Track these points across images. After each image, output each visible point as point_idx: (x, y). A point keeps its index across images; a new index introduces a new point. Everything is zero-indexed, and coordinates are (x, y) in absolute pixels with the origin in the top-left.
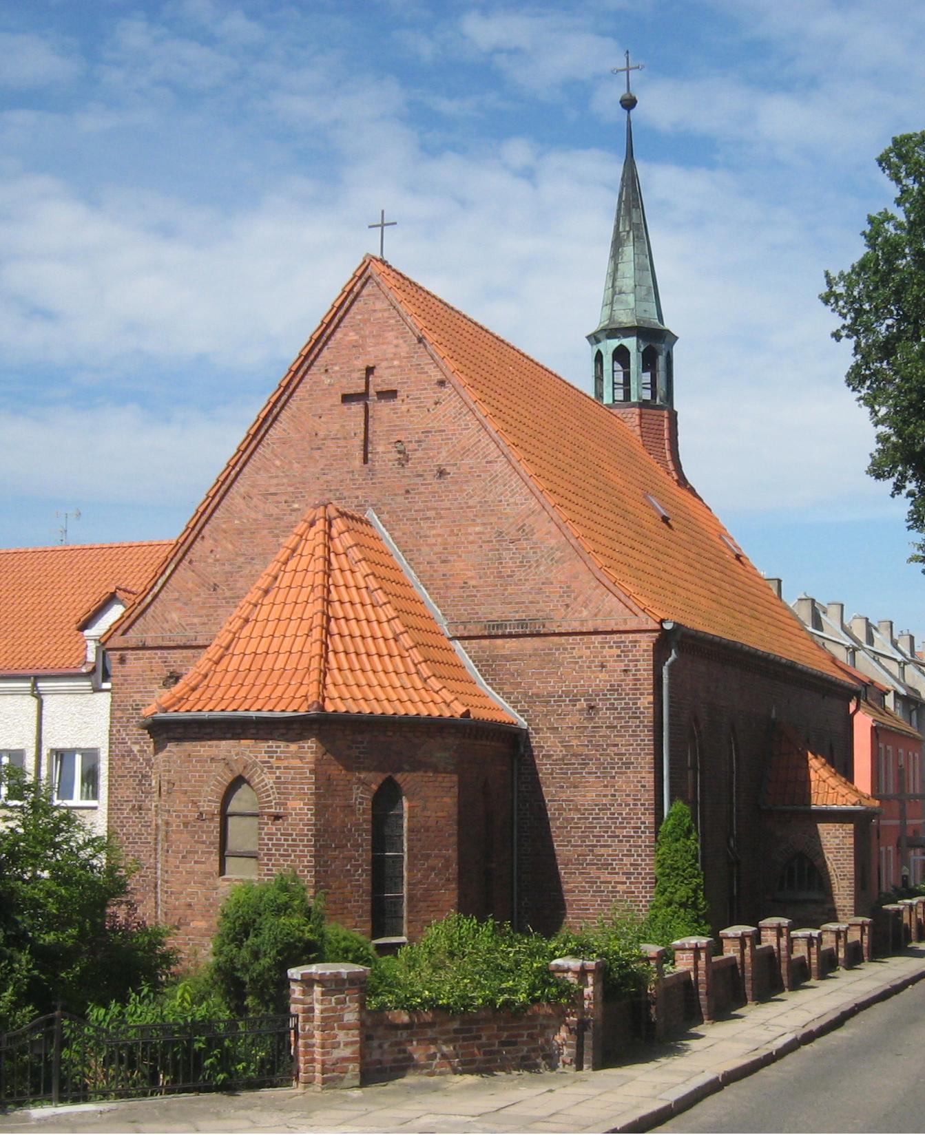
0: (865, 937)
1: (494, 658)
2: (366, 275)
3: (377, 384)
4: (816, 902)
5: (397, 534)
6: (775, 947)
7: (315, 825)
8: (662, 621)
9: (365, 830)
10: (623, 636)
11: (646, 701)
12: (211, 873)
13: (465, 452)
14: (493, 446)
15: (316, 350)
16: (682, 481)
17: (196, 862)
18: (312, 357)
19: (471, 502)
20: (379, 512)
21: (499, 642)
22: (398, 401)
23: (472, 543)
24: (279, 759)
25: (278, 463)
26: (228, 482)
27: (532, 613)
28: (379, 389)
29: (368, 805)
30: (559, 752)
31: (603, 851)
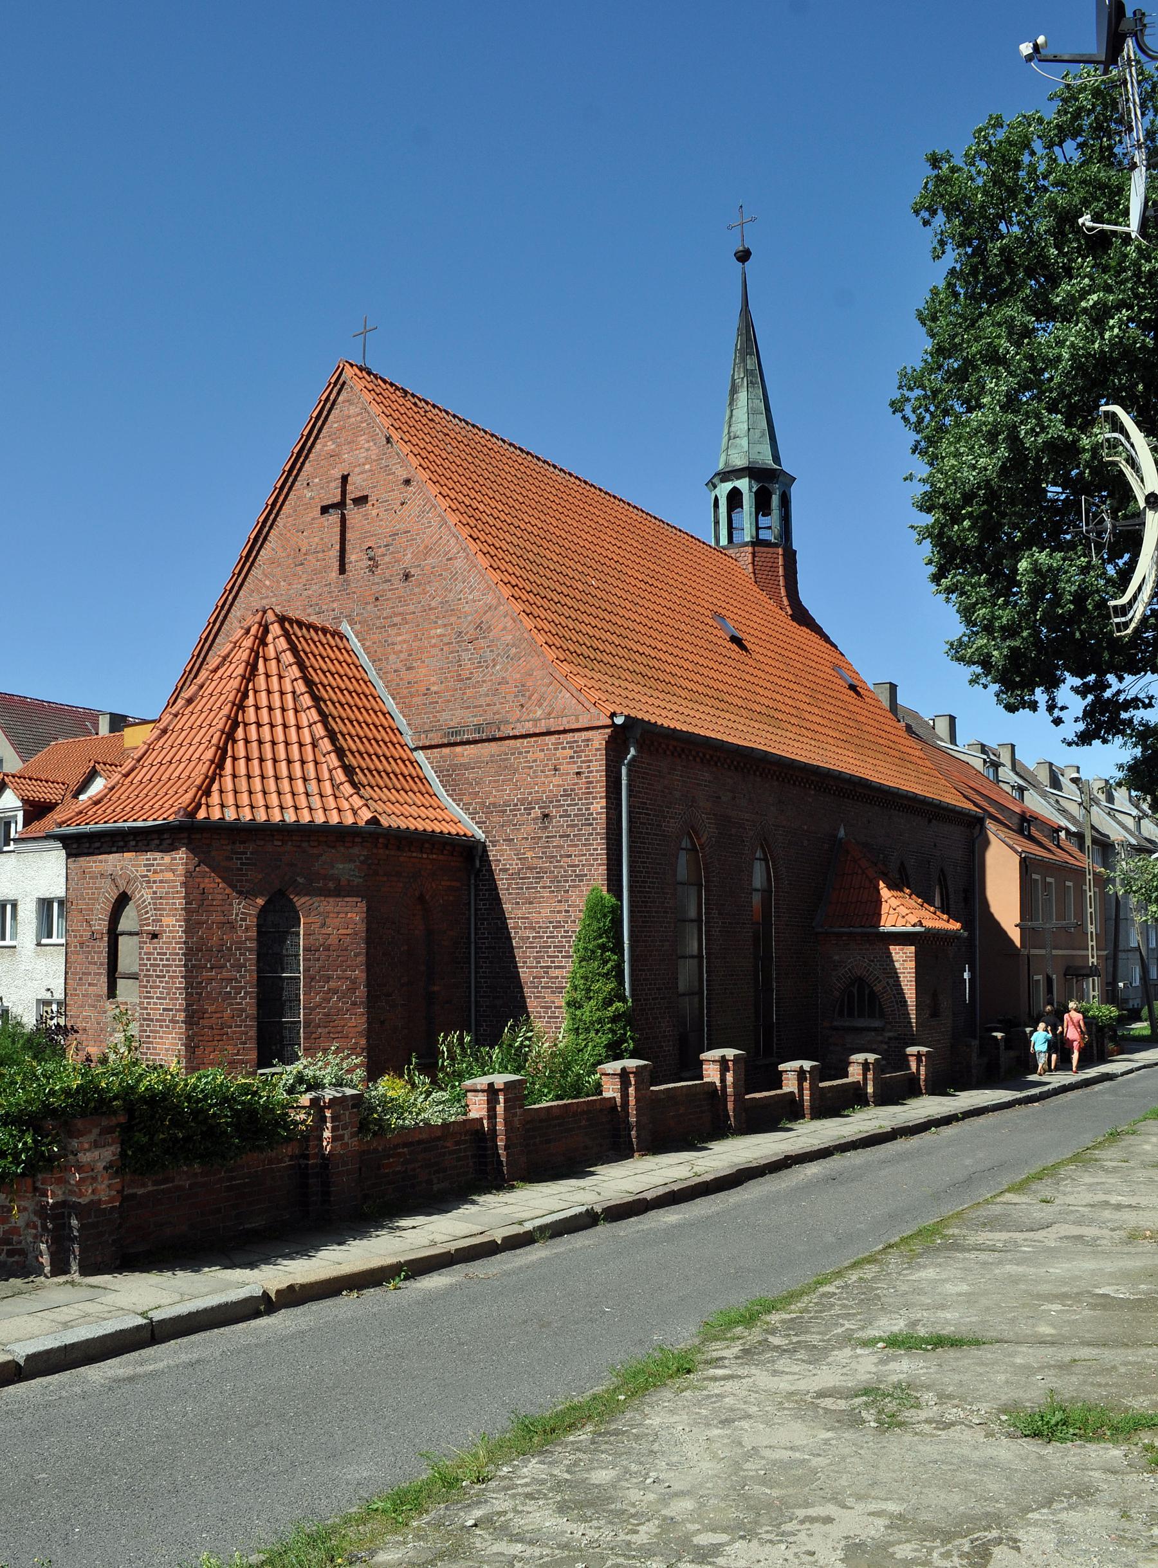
0: (922, 1069)
1: (454, 767)
2: (341, 381)
3: (353, 492)
4: (875, 1029)
5: (368, 644)
6: (718, 1084)
7: (185, 943)
8: (613, 715)
9: (250, 950)
10: (577, 734)
11: (599, 805)
12: (100, 996)
13: (428, 551)
14: (453, 541)
15: (299, 464)
16: (802, 617)
17: (90, 984)
18: (295, 472)
19: (433, 604)
20: (352, 623)
21: (458, 749)
22: (369, 506)
23: (434, 646)
24: (155, 872)
25: (267, 583)
26: (227, 606)
27: (489, 717)
28: (353, 496)
29: (252, 921)
30: (514, 865)
31: (557, 972)
